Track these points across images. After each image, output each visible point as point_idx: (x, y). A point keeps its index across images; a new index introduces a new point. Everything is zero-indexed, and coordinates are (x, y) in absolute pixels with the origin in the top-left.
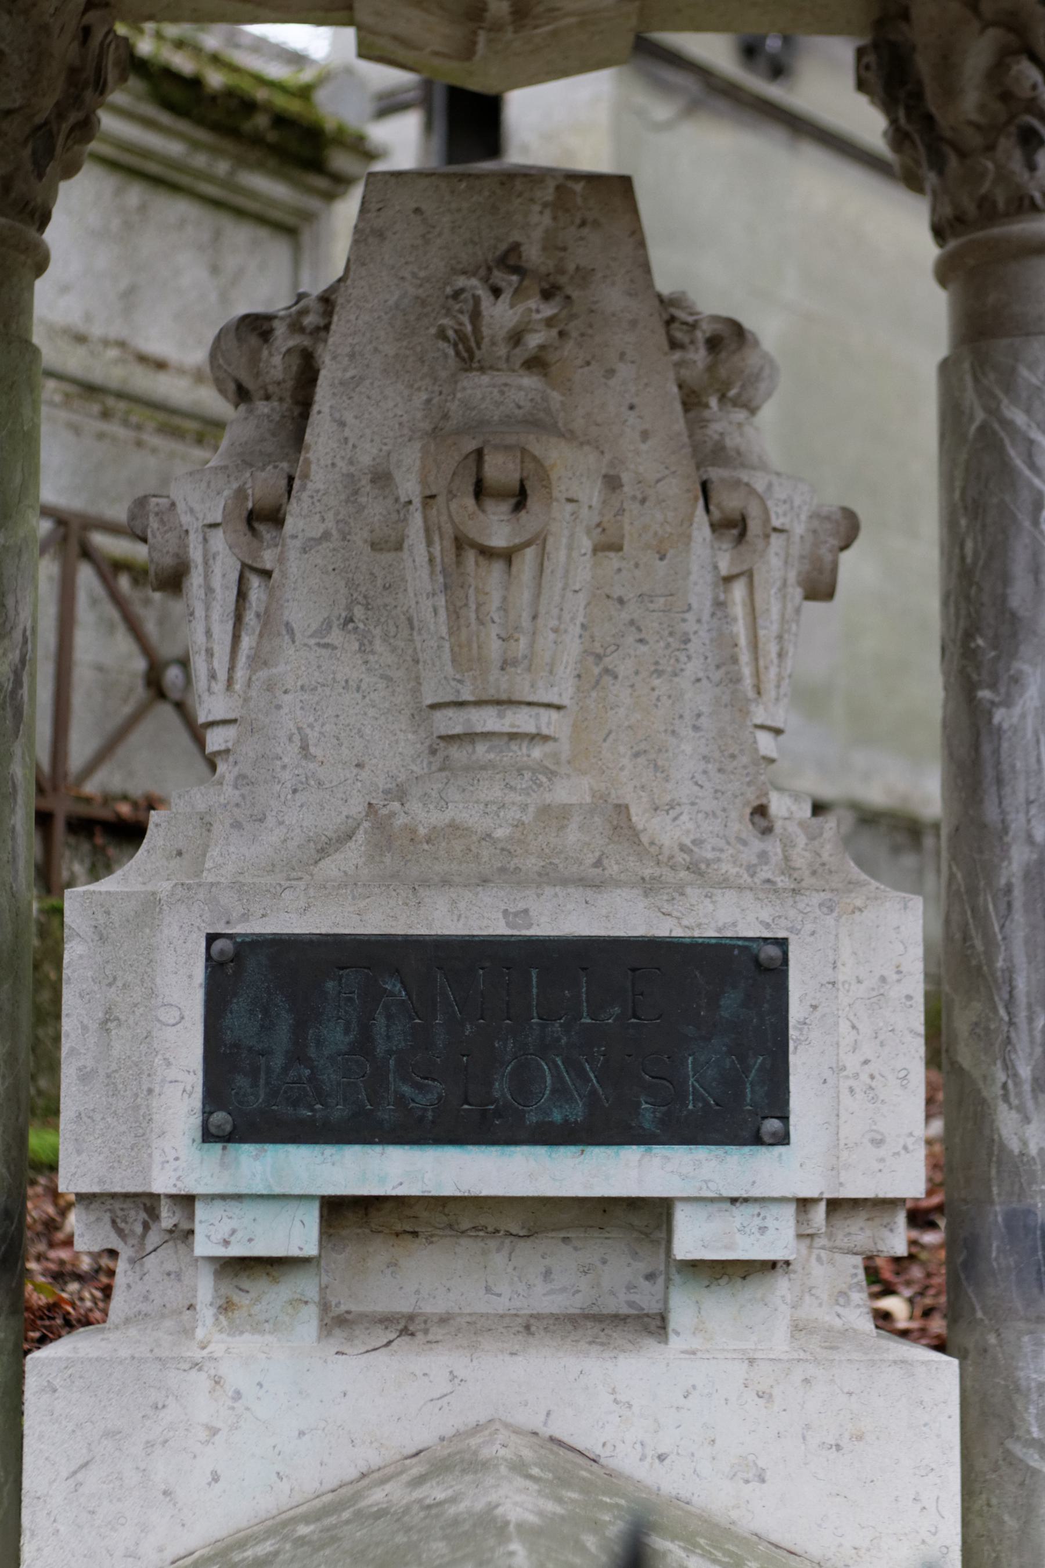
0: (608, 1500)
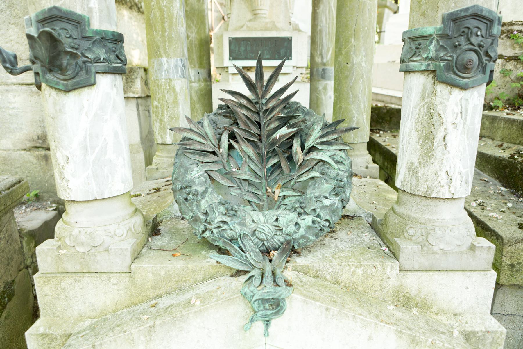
0: (166, 25)
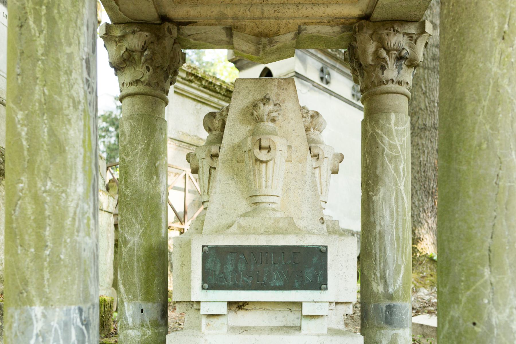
0: (47, 233)
